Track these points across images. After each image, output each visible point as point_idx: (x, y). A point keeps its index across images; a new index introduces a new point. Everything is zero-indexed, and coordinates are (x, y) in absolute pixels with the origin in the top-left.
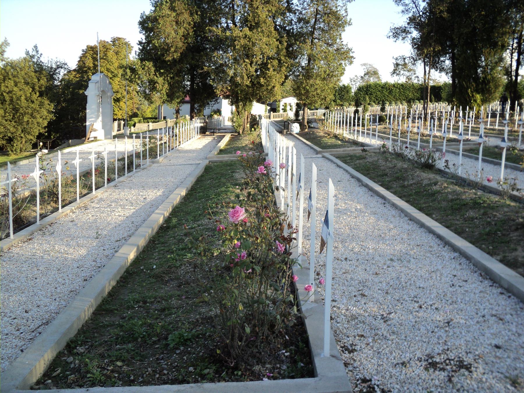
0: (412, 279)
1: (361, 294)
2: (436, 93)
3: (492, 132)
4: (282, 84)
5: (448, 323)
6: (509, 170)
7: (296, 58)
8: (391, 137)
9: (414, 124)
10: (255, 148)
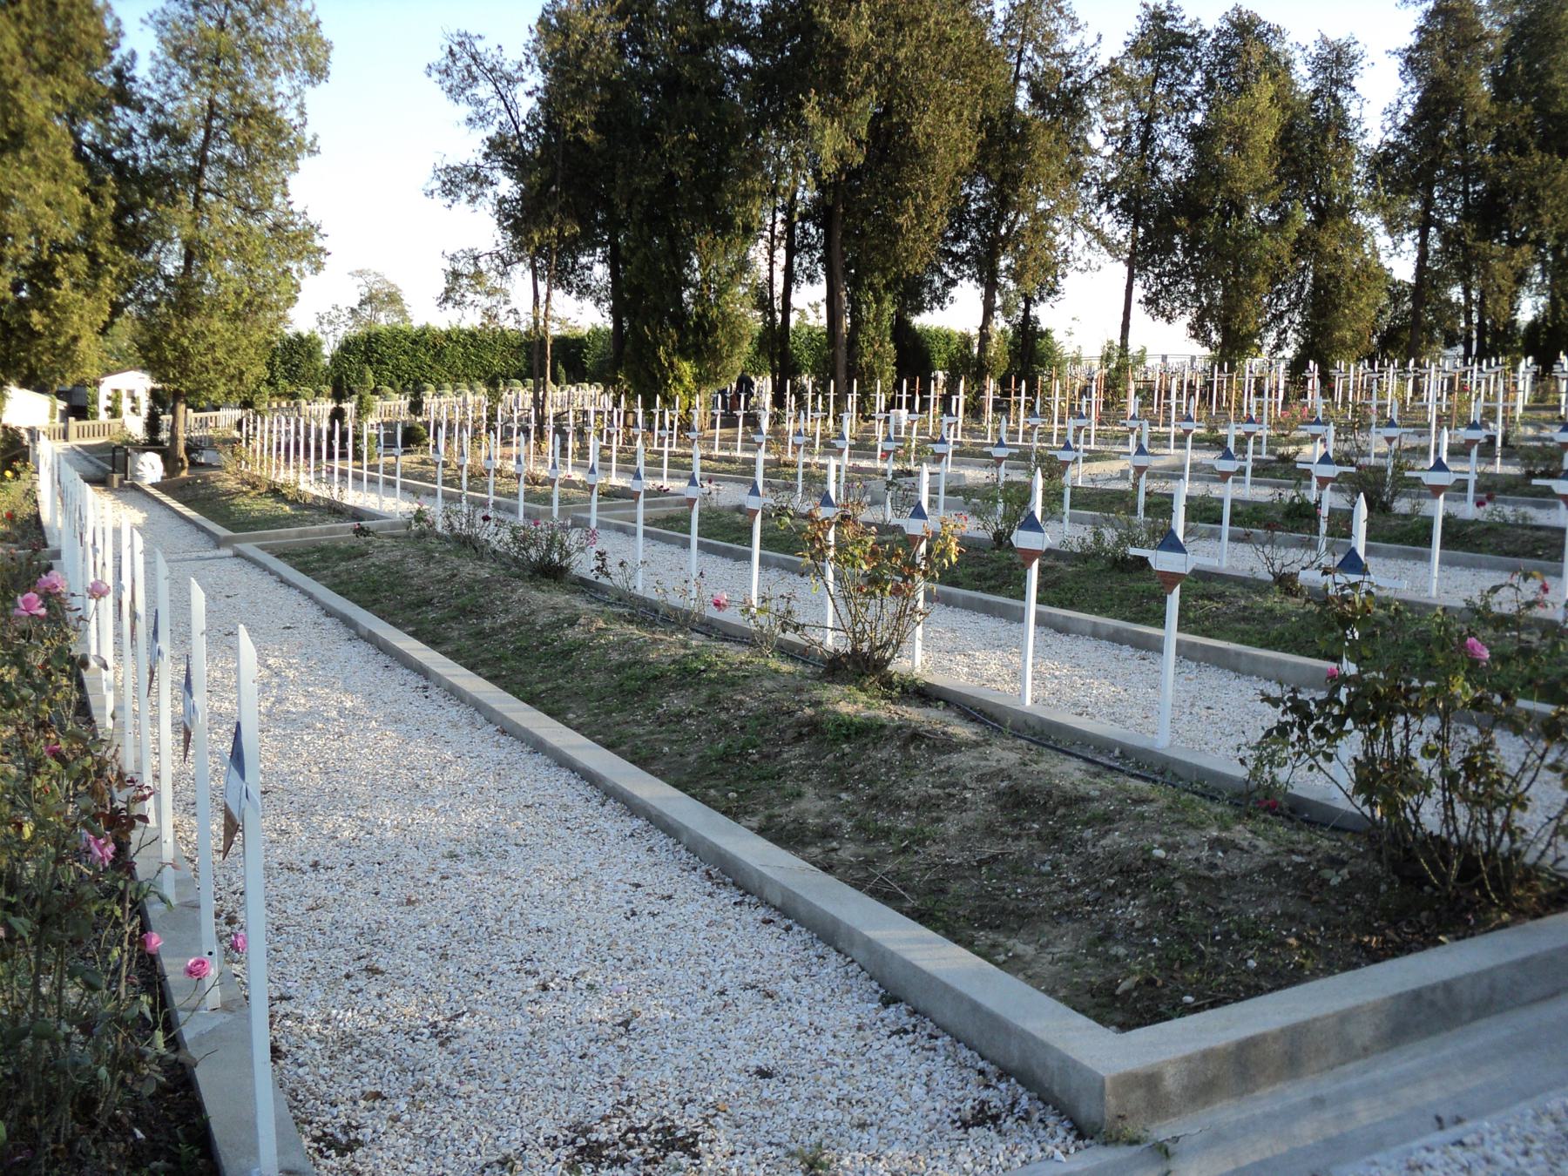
0: (516, 907)
1: (367, 969)
2: (571, 360)
3: (725, 466)
4: (103, 332)
5: (626, 1024)
6: (773, 574)
7: (147, 251)
8: (440, 487)
9: (507, 450)
10: (17, 533)
